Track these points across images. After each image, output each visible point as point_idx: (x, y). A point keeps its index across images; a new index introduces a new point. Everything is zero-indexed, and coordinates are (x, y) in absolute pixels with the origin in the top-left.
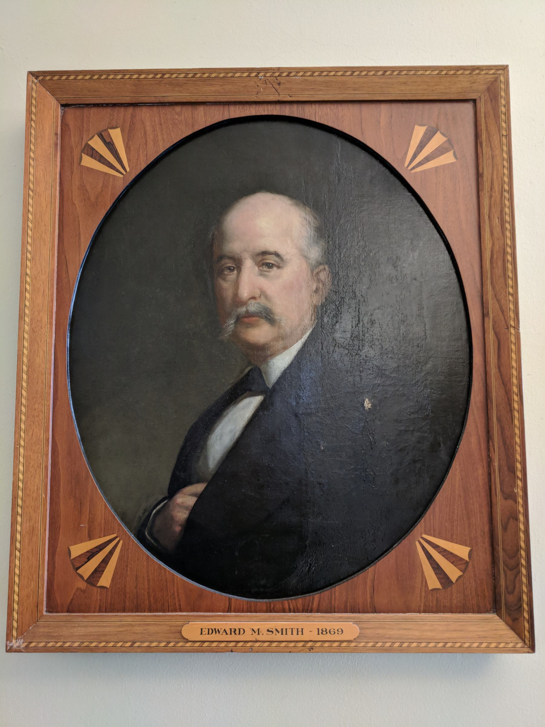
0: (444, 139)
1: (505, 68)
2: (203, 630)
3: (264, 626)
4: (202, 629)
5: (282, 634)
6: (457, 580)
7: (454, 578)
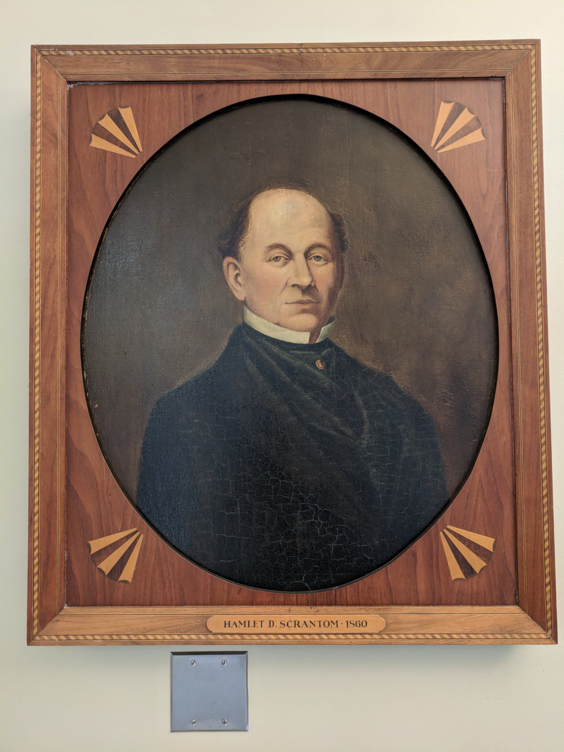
0: (471, 116)
1: (536, 43)
5: (245, 626)
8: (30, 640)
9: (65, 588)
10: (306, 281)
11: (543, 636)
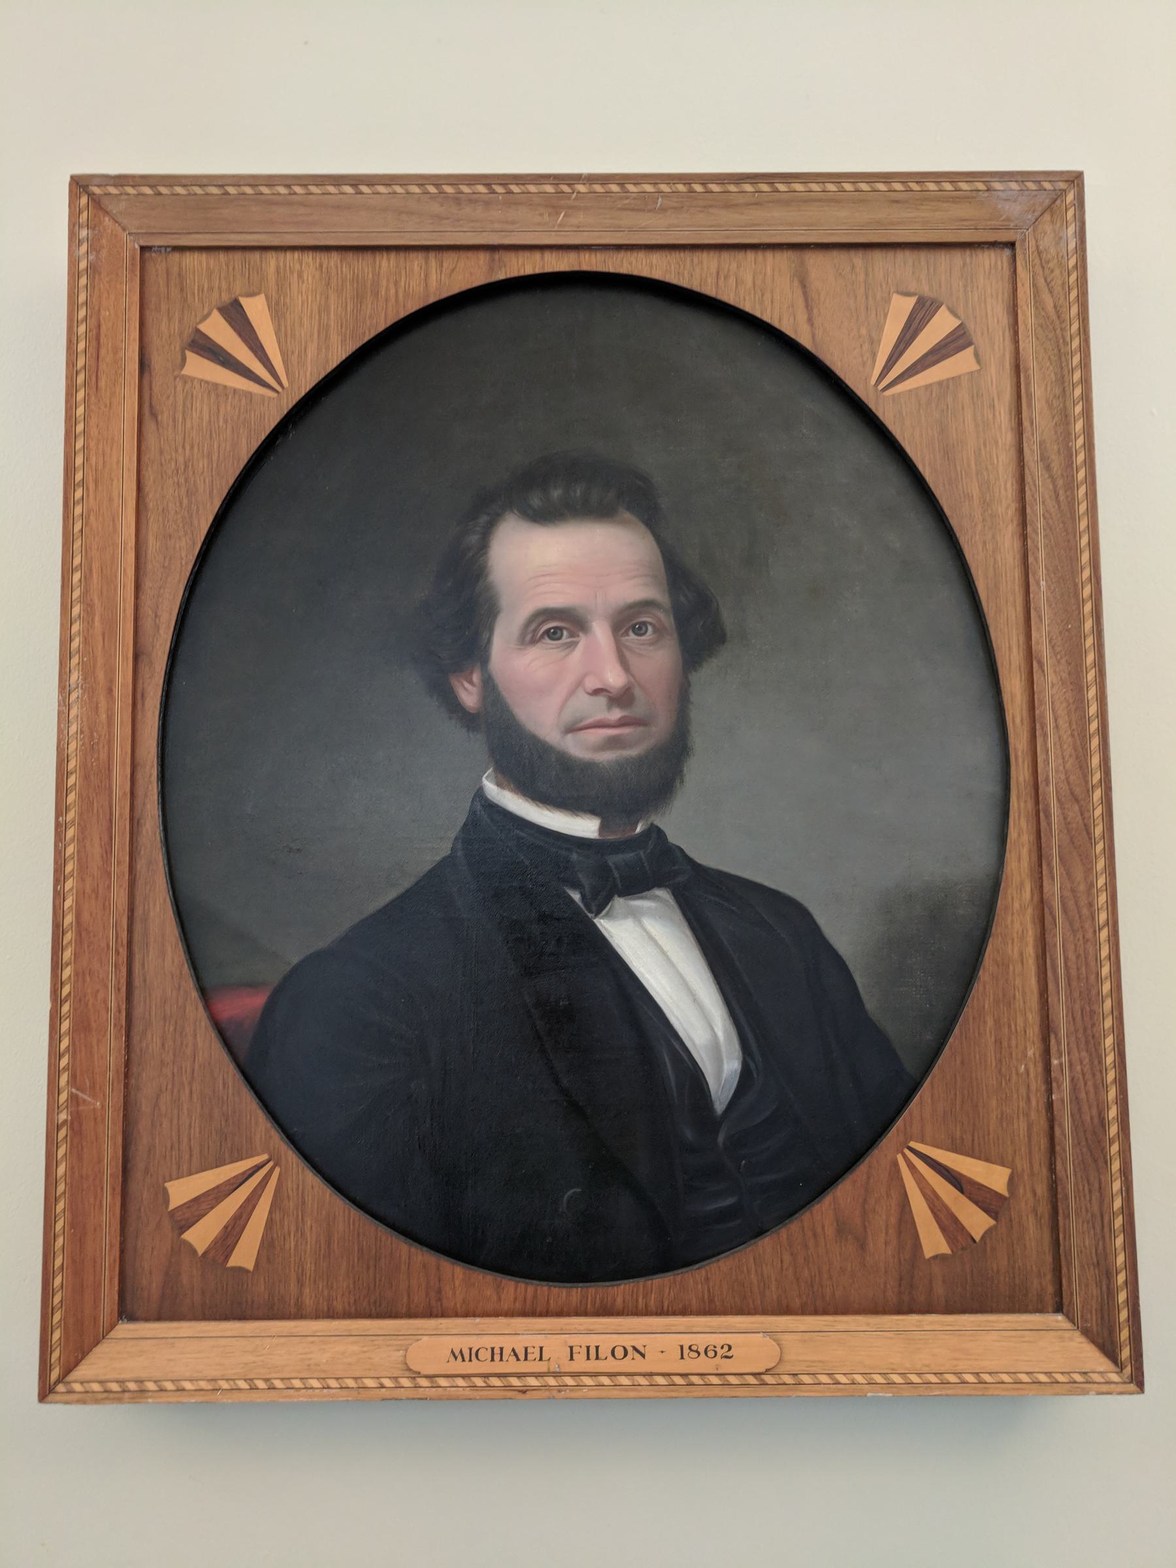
4: (571, 1348)
6: (956, 315)
8: (45, 1392)
11: (1114, 1377)
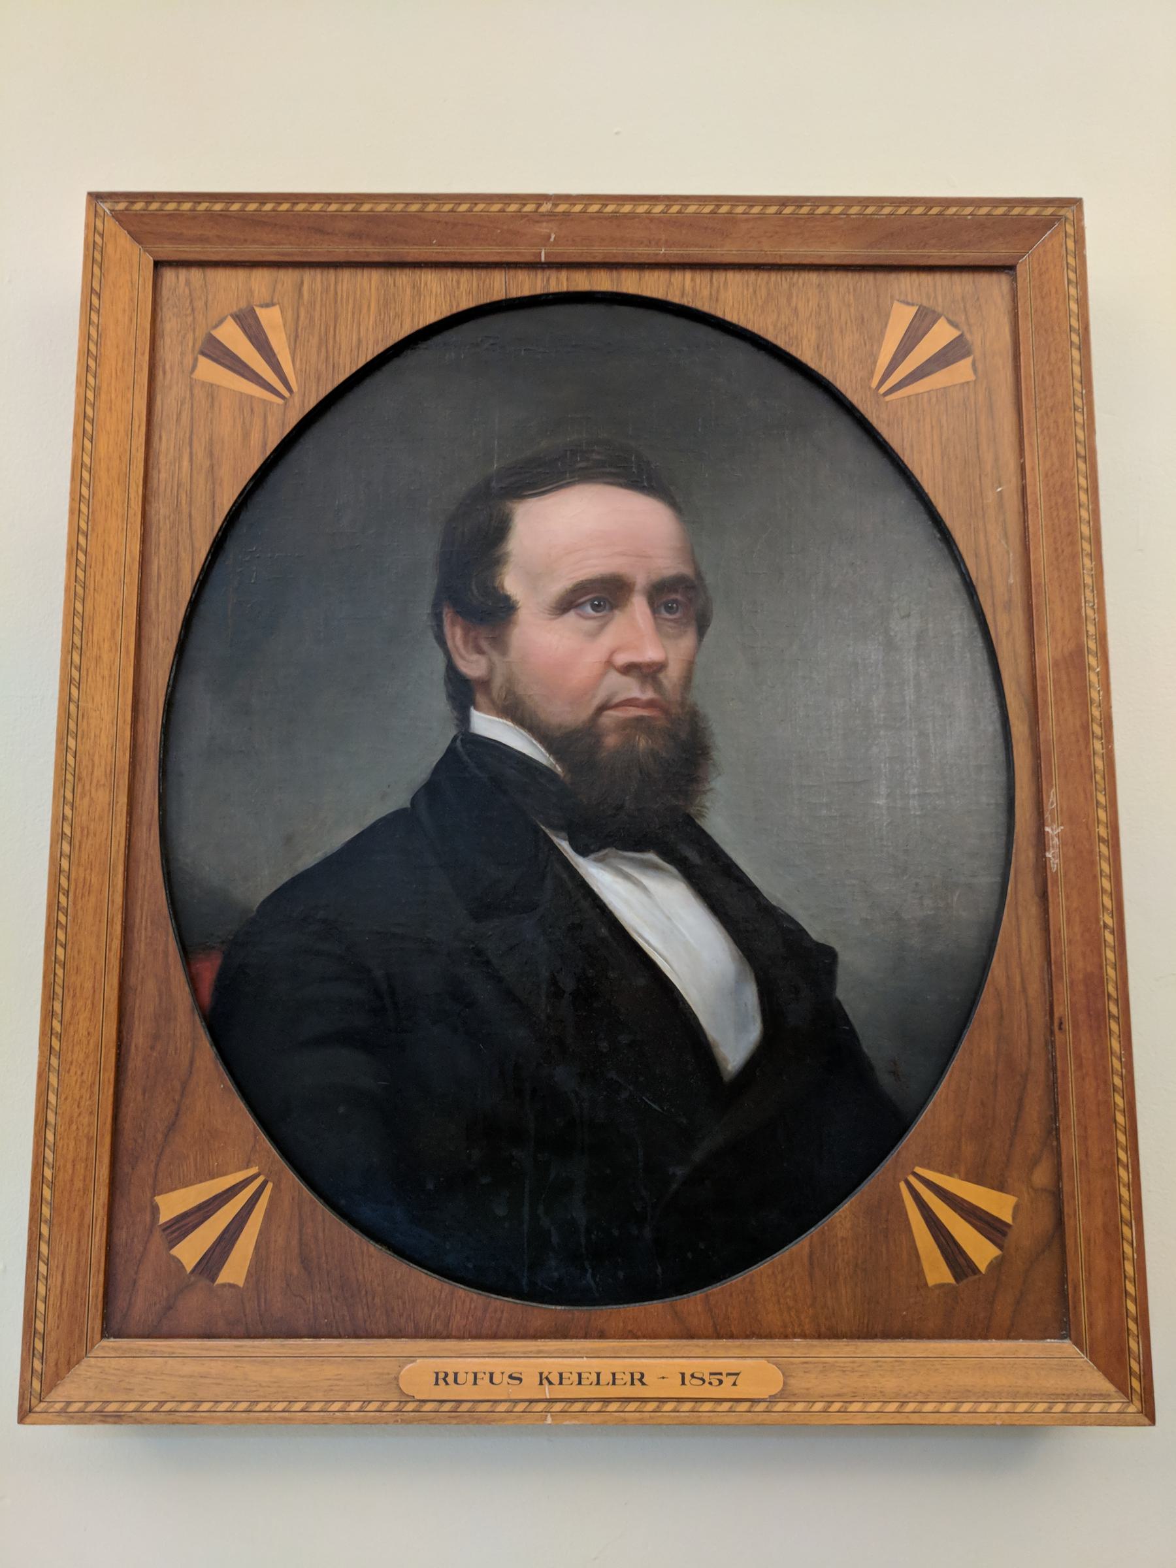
2: (479, 1376)
3: (530, 1368)
7: (225, 1277)
8: (25, 1414)
9: (111, 1292)
10: (651, 653)
